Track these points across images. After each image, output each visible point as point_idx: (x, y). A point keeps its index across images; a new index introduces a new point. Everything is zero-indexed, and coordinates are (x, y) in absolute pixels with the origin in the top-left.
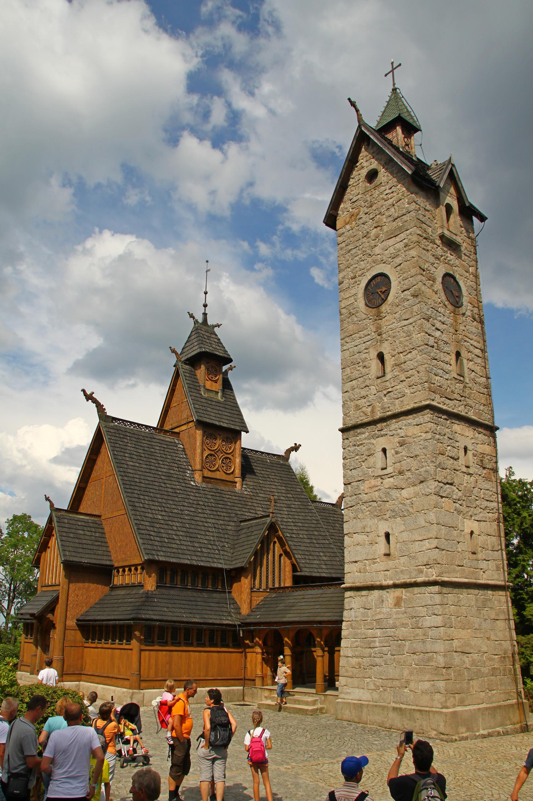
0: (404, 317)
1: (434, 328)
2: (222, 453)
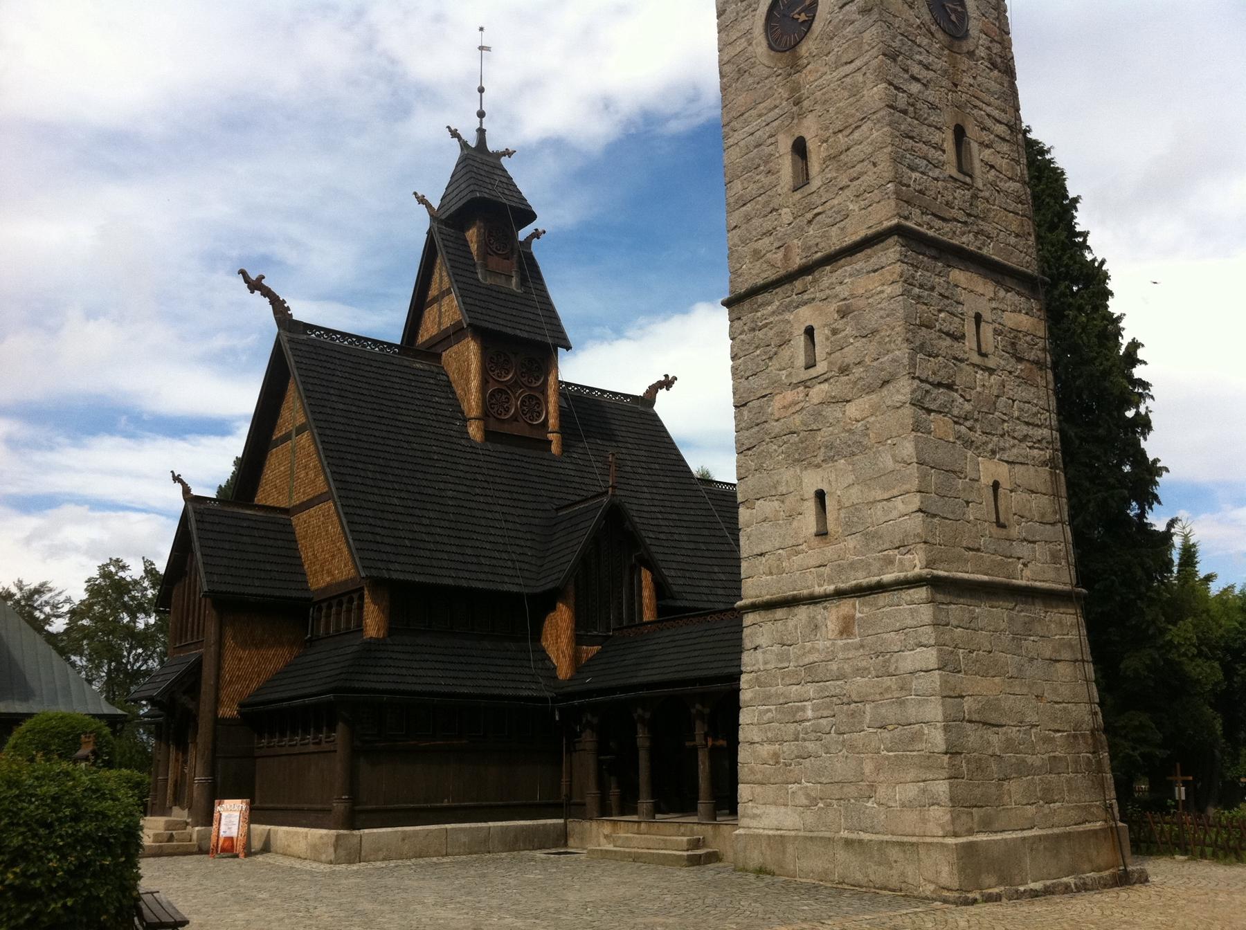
0: (844, 60)
1: (906, 76)
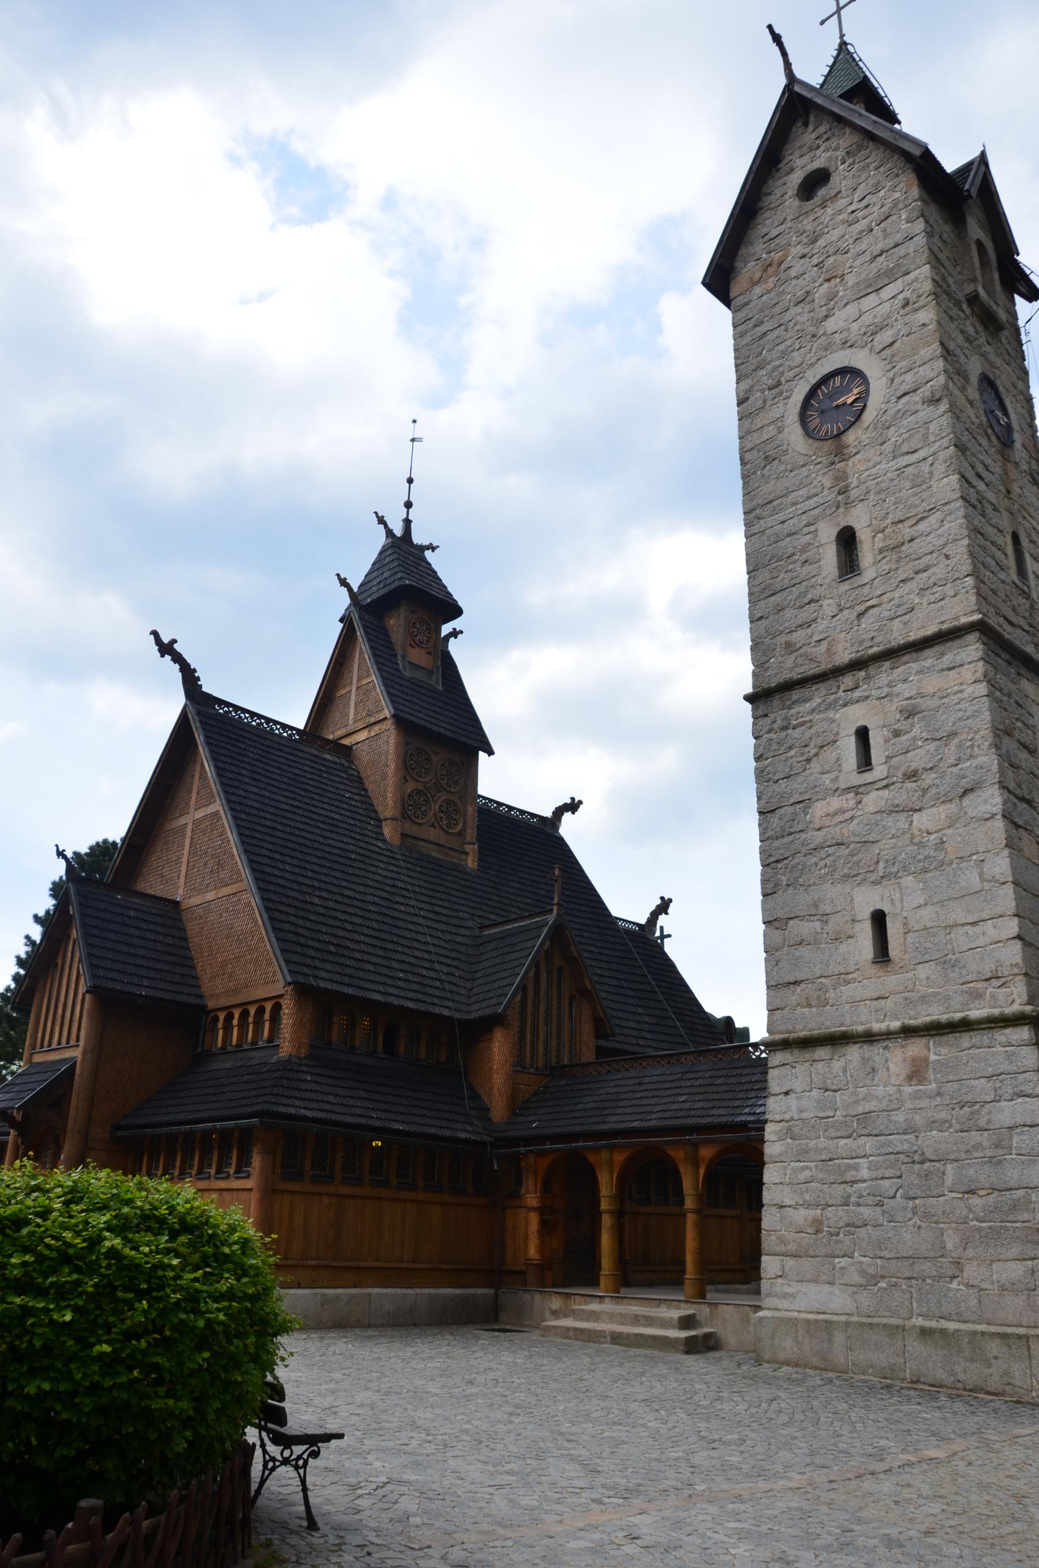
2: (440, 791)
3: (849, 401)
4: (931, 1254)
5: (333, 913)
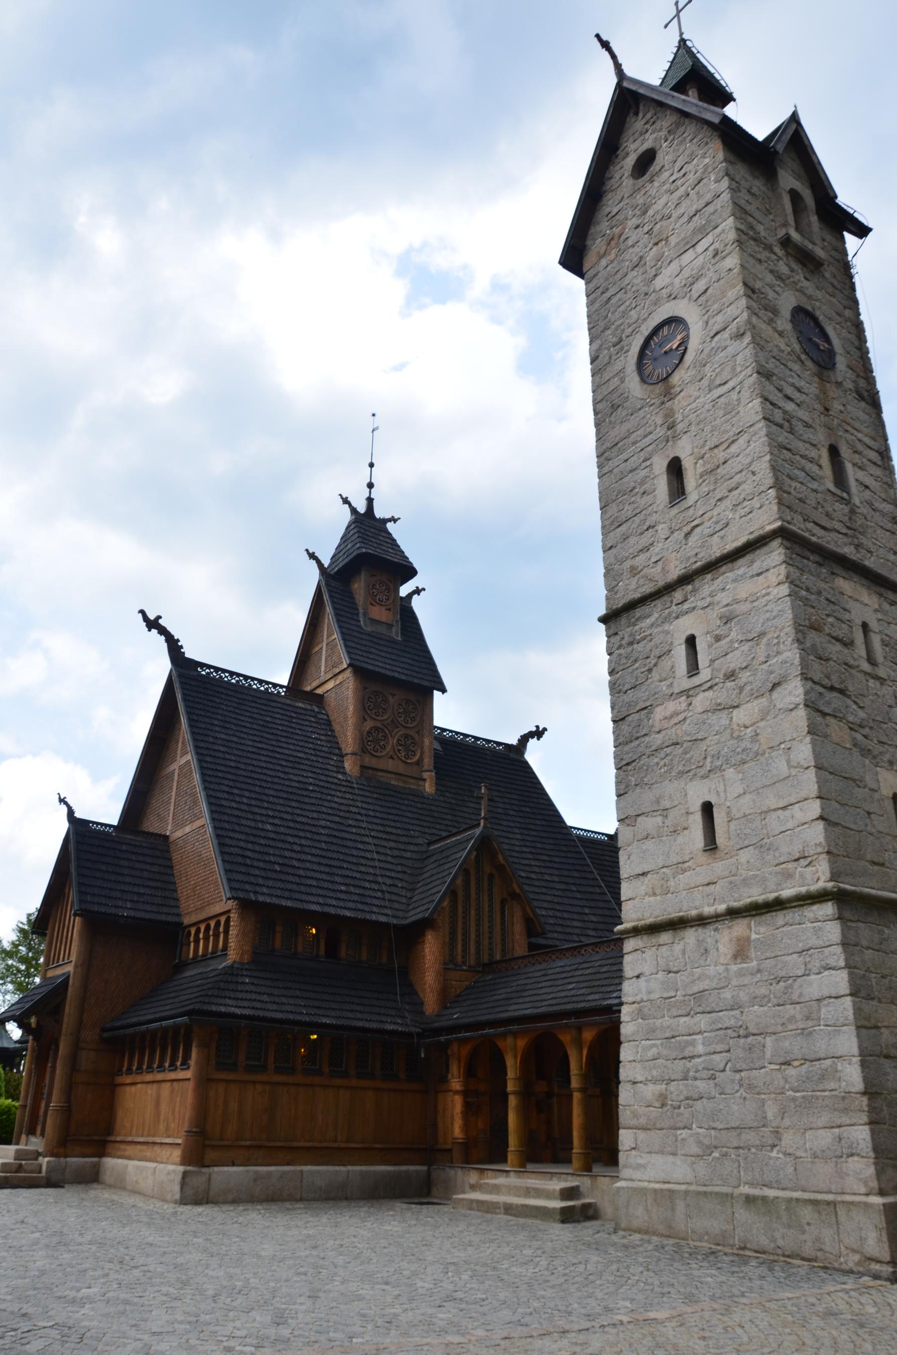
0: (718, 382)
3: (674, 347)
4: (755, 1124)
5: (282, 837)
